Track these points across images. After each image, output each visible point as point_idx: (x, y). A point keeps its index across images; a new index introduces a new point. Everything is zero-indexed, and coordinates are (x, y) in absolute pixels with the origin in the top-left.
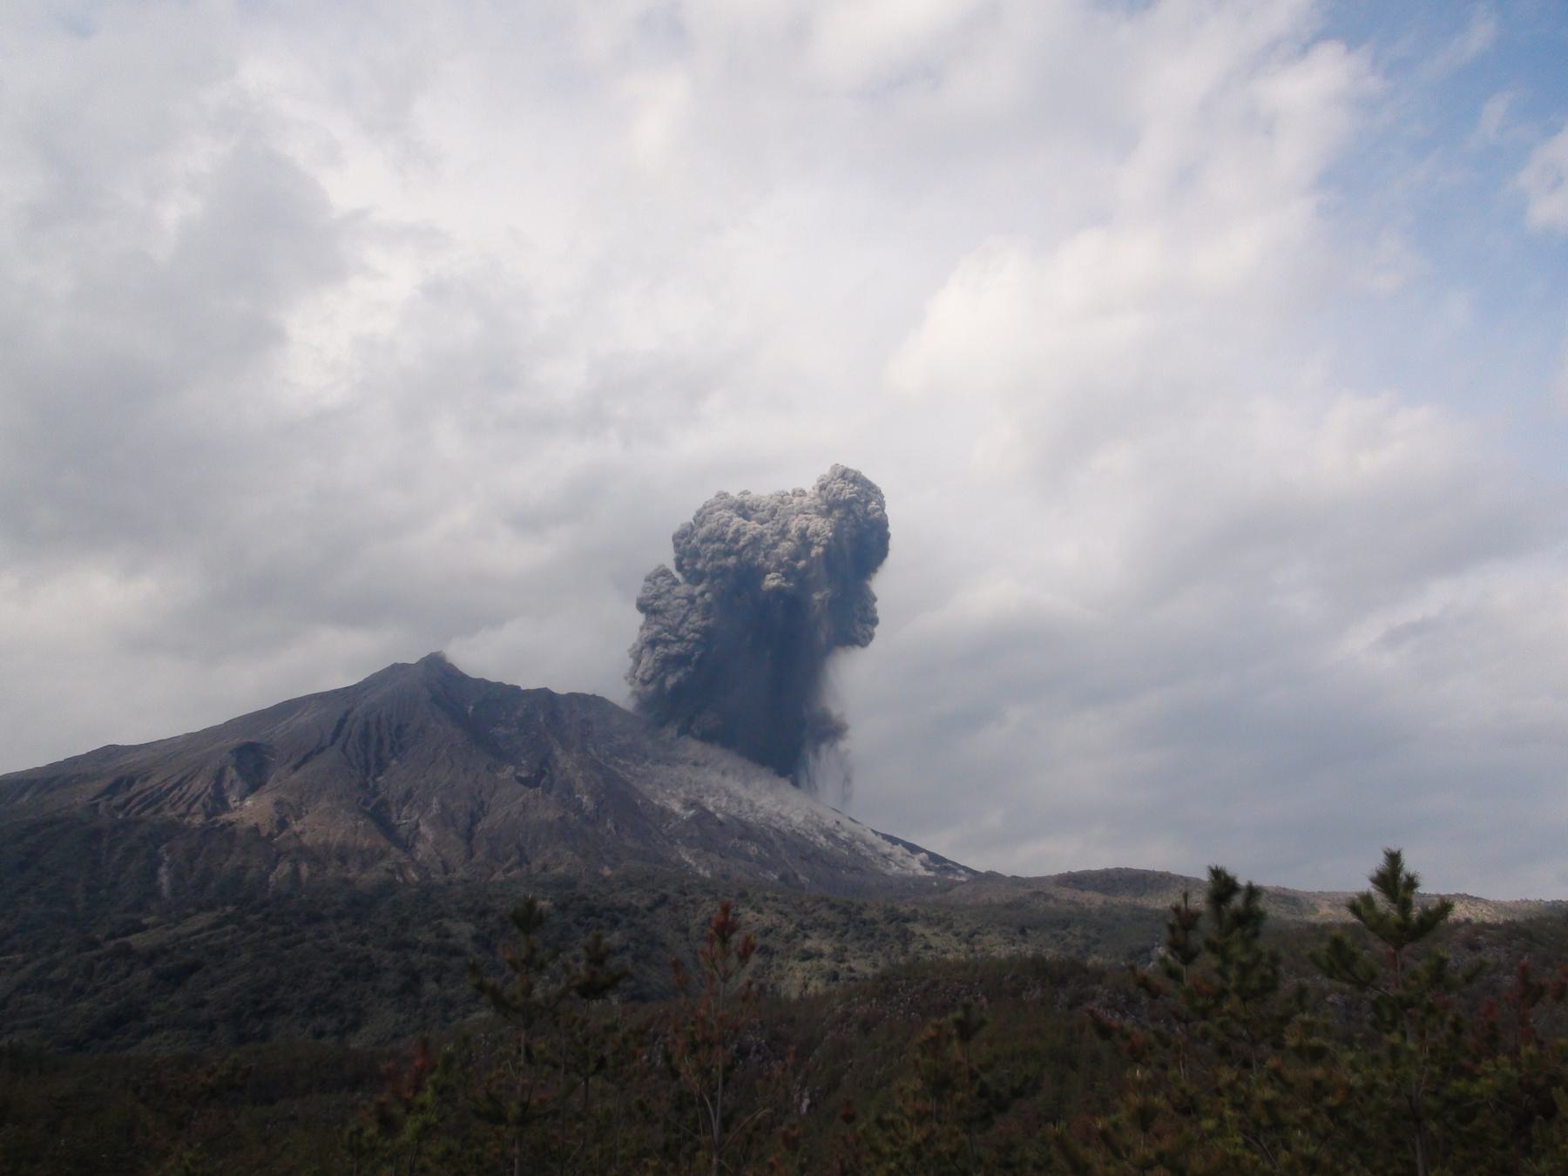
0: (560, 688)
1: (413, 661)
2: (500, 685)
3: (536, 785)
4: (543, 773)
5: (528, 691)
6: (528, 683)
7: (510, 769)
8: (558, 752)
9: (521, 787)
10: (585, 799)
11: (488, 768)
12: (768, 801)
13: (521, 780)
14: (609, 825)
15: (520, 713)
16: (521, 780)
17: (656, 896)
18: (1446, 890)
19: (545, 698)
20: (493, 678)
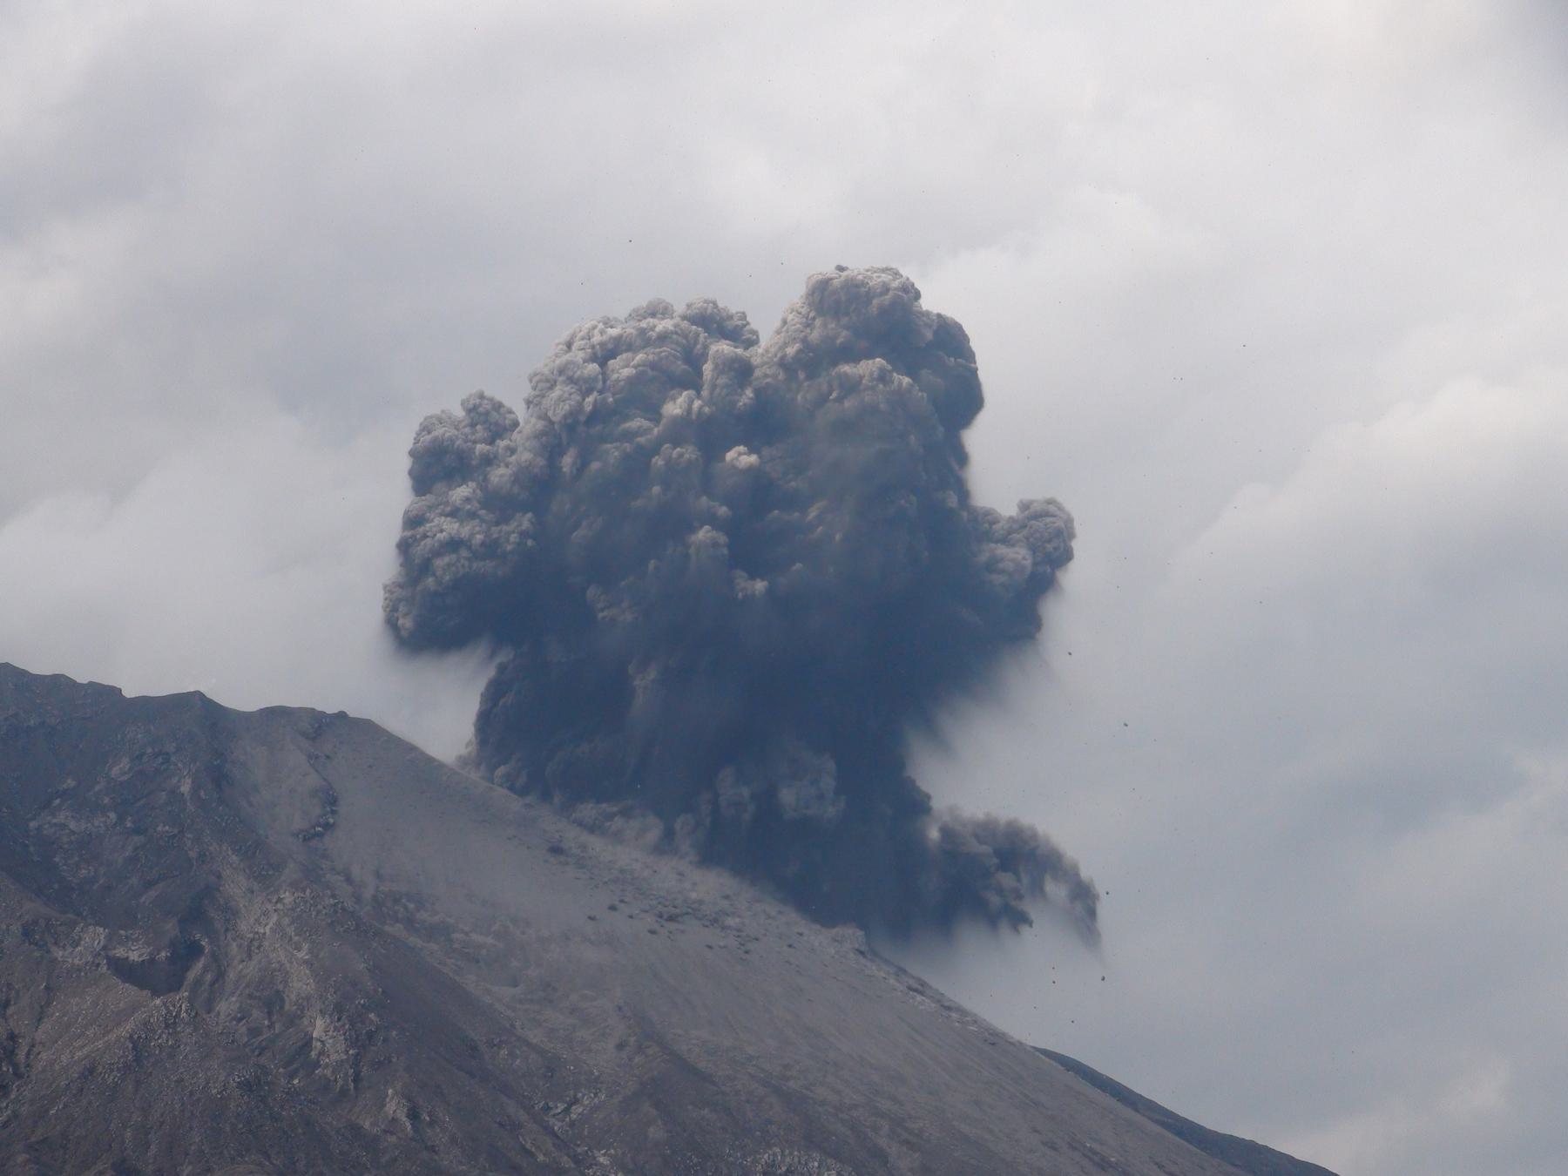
0: (241, 690)
1: (129, 692)
2: (58, 684)
3: (174, 985)
4: (194, 951)
5: (144, 701)
6: (140, 676)
7: (94, 937)
8: (236, 886)
9: (127, 993)
10: (319, 1028)
11: (27, 933)
12: (784, 987)
13: (124, 970)
14: (394, 1107)
15: (120, 769)
16: (124, 970)
17: (23, 1069)
18: (1064, 827)
19: (195, 721)
20: (40, 665)
